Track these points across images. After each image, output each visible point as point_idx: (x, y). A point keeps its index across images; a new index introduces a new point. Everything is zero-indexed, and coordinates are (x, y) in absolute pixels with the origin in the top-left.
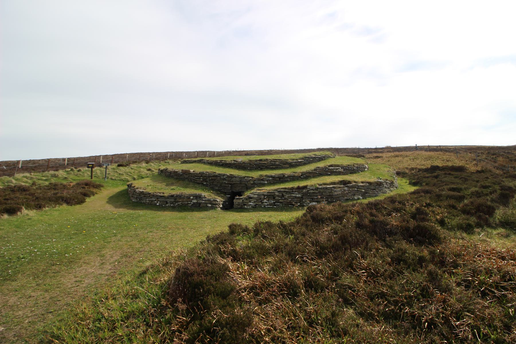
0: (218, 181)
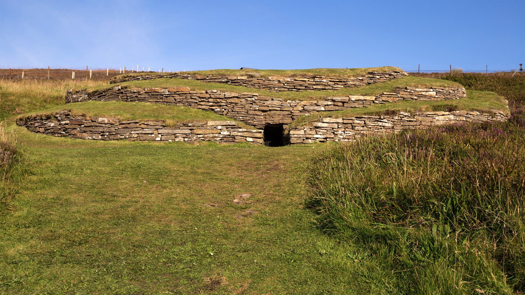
0: (242, 106)
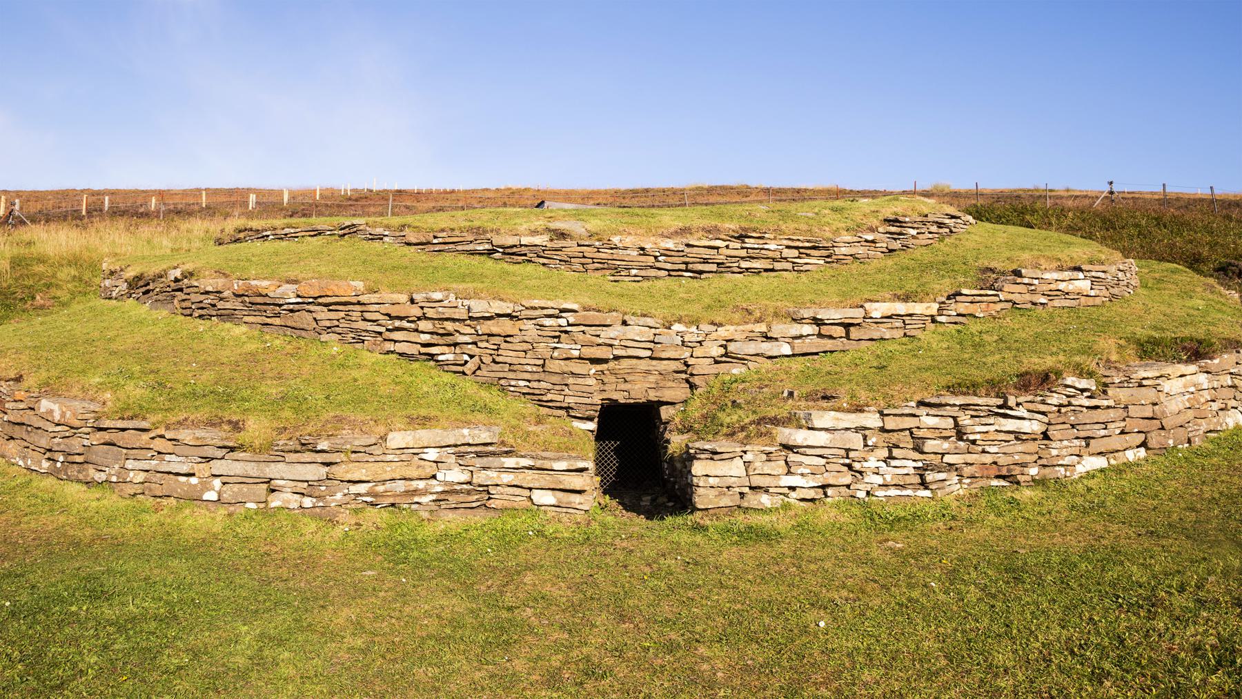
0: (526, 346)
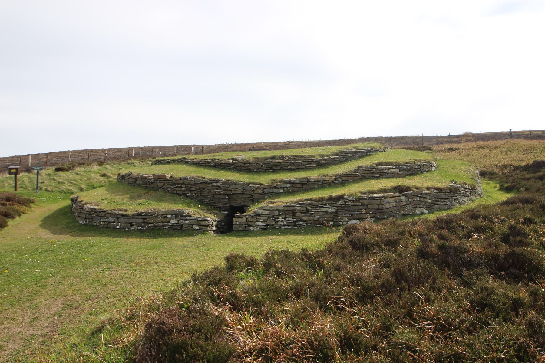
0: (208, 191)
